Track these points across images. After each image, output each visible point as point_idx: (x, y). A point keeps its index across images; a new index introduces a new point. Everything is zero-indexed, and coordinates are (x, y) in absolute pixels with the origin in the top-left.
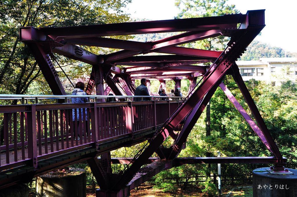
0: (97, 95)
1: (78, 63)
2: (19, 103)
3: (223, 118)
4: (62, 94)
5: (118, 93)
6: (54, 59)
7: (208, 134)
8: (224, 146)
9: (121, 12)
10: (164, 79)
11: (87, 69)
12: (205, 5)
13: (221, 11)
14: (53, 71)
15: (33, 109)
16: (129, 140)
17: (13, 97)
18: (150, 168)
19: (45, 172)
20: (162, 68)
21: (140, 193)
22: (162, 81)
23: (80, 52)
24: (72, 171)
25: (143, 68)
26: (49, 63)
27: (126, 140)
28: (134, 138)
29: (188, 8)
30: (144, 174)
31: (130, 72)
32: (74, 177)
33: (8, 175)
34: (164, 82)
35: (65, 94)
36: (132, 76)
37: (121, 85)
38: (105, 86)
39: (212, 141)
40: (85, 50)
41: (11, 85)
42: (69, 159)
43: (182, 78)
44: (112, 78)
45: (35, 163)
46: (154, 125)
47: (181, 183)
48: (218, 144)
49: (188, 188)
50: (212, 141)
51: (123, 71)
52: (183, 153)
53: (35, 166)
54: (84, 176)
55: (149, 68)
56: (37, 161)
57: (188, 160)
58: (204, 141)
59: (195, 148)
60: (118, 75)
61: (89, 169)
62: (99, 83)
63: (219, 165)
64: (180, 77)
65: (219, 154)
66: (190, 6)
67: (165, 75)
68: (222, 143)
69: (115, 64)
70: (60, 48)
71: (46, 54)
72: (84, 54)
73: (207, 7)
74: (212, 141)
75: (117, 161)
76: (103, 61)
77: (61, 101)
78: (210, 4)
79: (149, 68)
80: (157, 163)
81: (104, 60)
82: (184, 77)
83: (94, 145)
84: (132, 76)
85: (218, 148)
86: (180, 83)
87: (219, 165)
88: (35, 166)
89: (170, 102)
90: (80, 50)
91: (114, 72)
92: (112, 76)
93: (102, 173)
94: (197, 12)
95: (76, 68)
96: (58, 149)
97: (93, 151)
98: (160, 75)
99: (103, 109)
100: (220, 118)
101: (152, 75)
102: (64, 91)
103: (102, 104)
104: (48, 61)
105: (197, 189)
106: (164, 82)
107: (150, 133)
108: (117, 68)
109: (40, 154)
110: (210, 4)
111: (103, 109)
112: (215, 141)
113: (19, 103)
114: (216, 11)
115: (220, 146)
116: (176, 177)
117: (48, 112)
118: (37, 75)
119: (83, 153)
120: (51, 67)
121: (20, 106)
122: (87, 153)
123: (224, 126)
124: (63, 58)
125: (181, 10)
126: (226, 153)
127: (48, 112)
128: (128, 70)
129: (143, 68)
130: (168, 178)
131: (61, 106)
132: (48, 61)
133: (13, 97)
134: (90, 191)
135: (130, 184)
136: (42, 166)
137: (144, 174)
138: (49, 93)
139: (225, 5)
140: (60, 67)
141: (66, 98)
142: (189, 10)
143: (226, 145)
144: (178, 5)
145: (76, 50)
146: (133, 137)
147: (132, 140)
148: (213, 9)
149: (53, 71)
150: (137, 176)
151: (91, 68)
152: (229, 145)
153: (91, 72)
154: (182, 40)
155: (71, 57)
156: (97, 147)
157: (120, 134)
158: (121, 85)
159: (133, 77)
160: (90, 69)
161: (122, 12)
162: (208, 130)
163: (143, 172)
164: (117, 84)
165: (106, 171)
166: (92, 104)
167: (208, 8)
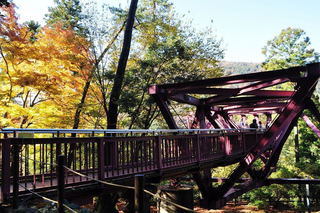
0: (200, 129)
1: (185, 105)
2: (129, 135)
3: (311, 146)
4: (175, 129)
5: (216, 126)
6: (169, 103)
7: (297, 160)
8: (313, 171)
9: (216, 66)
10: (258, 114)
11: (192, 109)
12: (288, 51)
13: (302, 55)
14: (169, 113)
15: (159, 138)
16: (223, 161)
17: (142, 131)
18: (243, 185)
19: (166, 179)
20: (252, 106)
21: (238, 208)
22: (255, 115)
23: (187, 98)
24: (183, 187)
25: (236, 107)
26: (167, 107)
27: (221, 161)
28: (227, 160)
29: (273, 54)
30: (238, 190)
31: (226, 110)
32: (184, 190)
33: (147, 177)
34: (258, 116)
35: (178, 128)
36: (229, 112)
37: (219, 121)
38: (207, 121)
39: (301, 166)
40: (190, 96)
41: (140, 123)
42: (181, 171)
43: (272, 112)
44: (212, 115)
45: (161, 172)
46: (244, 150)
47: (273, 202)
48: (307, 169)
49: (278, 205)
50: (301, 166)
51: (221, 109)
52: (273, 176)
53: (161, 173)
54: (192, 190)
55: (239, 106)
56: (162, 171)
57: (278, 181)
58: (293, 166)
59: (285, 170)
60: (217, 113)
61: (196, 187)
62: (202, 120)
63: (307, 186)
64: (270, 111)
65: (306, 176)
66: (275, 53)
67: (256, 111)
68: (311, 169)
69: (214, 105)
70: (173, 97)
71: (164, 101)
72: (190, 98)
73: (290, 52)
74: (301, 166)
75: (216, 180)
76: (204, 103)
77: (175, 133)
78: (292, 49)
79: (239, 106)
80: (249, 182)
81: (205, 102)
82: (273, 112)
83: (197, 163)
84: (229, 112)
85: (307, 173)
86: (271, 117)
87: (307, 186)
88: (161, 173)
89: (257, 133)
90: (187, 96)
91: (213, 111)
92: (211, 114)
93: (205, 186)
94: (282, 57)
95: (185, 109)
96: (174, 164)
97: (197, 167)
98: (252, 111)
99: (208, 138)
100: (309, 145)
101: (242, 111)
102: (177, 126)
103: (203, 135)
104: (166, 106)
105: (288, 207)
106: (258, 116)
107: (240, 156)
108: (216, 108)
109: (164, 166)
110: (292, 49)
111: (208, 138)
112: (304, 166)
113: (129, 135)
114: (298, 55)
115: (308, 171)
116: (268, 196)
117: (164, 141)
118: (158, 115)
119: (190, 168)
120: (167, 110)
121: (129, 137)
122: (193, 168)
123: (314, 153)
124: (176, 102)
125: (268, 56)
126: (315, 177)
127: (164, 141)
128: (224, 109)
129: (236, 107)
130: (260, 196)
131: (176, 136)
132: (166, 106)
133: (142, 131)
134: (197, 204)
135: (226, 195)
136: (165, 174)
137: (238, 190)
138: (166, 128)
139: (305, 50)
140: (173, 109)
141: (179, 131)
142: (275, 55)
143: (315, 170)
144: (264, 53)
145: (184, 96)
146: (226, 159)
147: (226, 161)
148: (295, 54)
149: (169, 113)
150: (231, 191)
151: (196, 108)
152: (317, 170)
153: (195, 111)
154: (260, 86)
155: (180, 102)
156: (200, 165)
157: (214, 157)
158: (219, 121)
159: (230, 113)
160: (195, 109)
161: (217, 66)
162: (298, 156)
163: (237, 189)
164: (216, 121)
165: (208, 185)
166: (196, 135)
167: (291, 53)
